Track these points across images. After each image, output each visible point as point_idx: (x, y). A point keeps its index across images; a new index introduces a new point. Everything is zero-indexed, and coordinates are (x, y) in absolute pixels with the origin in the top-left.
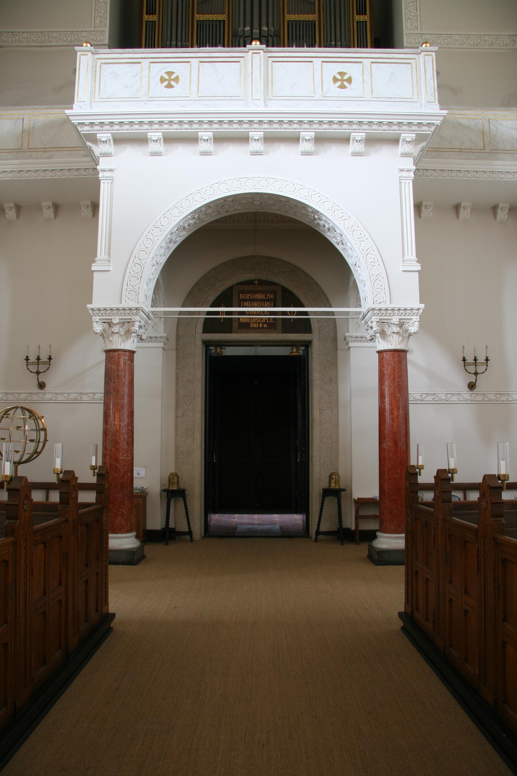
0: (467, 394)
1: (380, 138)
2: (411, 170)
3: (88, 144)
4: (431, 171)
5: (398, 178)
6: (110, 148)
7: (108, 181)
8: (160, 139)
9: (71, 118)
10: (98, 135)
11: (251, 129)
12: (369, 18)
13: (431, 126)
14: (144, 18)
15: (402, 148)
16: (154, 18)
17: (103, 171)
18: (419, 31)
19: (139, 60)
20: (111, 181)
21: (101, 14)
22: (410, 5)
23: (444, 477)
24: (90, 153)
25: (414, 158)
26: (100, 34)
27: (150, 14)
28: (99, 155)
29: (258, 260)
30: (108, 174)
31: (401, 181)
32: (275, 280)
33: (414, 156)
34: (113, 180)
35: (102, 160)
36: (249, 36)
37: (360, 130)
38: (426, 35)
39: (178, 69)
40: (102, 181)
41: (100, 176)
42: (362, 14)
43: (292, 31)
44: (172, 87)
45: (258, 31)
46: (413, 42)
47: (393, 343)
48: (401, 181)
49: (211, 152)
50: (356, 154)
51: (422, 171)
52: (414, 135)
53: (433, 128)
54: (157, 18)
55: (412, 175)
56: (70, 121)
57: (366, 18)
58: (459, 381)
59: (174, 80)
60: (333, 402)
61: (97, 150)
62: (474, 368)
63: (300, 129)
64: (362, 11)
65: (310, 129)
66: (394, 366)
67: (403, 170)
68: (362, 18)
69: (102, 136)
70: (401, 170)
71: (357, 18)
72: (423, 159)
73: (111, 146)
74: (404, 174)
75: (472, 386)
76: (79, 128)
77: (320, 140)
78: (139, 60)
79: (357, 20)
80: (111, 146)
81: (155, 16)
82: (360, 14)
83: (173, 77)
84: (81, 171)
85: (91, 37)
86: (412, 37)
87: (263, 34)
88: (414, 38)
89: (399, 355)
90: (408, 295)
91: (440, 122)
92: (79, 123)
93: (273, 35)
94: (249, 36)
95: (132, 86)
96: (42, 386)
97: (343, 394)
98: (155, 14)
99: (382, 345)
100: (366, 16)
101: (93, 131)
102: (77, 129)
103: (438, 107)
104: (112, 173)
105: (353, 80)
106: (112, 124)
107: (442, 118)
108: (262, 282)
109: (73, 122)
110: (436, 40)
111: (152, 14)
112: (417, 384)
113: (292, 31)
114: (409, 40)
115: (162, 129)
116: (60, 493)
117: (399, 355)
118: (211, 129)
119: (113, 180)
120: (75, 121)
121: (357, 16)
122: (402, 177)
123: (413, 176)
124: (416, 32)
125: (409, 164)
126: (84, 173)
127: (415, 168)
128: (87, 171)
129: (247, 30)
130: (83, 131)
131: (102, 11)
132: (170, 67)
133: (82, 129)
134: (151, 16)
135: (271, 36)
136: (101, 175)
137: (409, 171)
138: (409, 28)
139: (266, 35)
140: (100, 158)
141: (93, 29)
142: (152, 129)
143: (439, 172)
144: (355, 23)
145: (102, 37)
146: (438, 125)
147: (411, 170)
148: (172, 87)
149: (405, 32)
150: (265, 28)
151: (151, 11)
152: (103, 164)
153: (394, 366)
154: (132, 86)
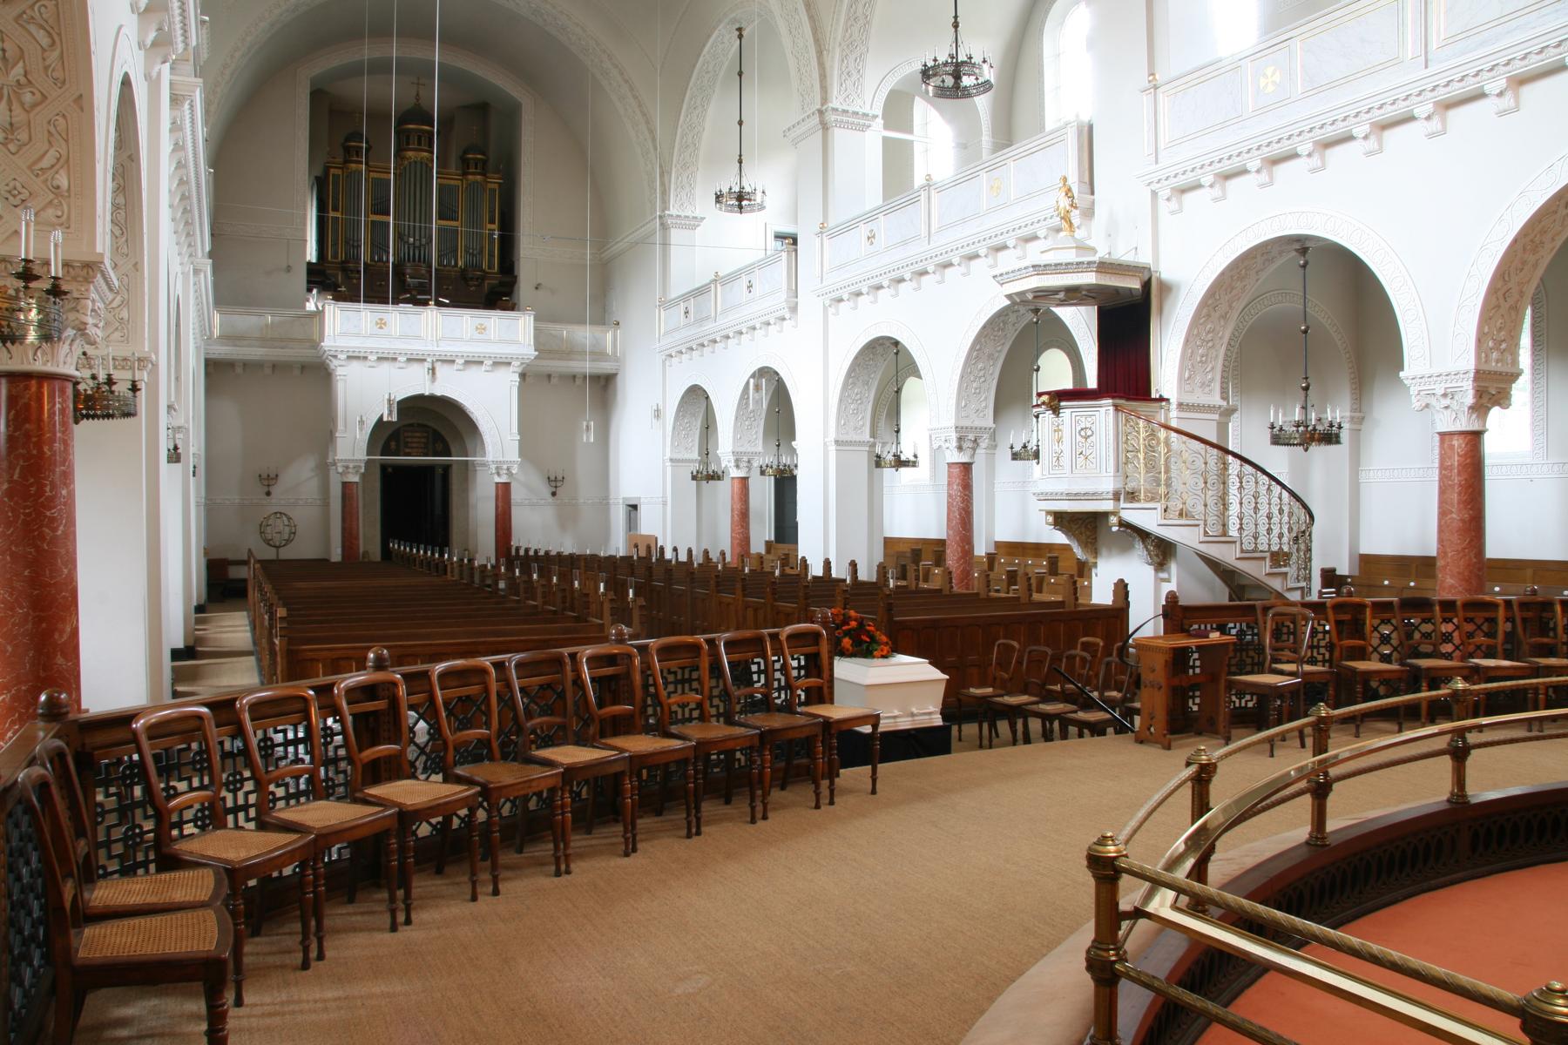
0: (550, 499)
1: (500, 363)
16: (338, 215)
23: (547, 553)
29: (428, 433)
32: (430, 424)
47: (504, 479)
58: (546, 491)
60: (466, 504)
62: (555, 484)
64: (492, 222)
66: (504, 491)
75: (554, 494)
89: (507, 486)
90: (513, 454)
96: (268, 494)
97: (472, 500)
99: (497, 480)
108: (419, 425)
112: (517, 495)
116: (941, 543)
117: (507, 486)
151: (335, 209)
153: (504, 491)
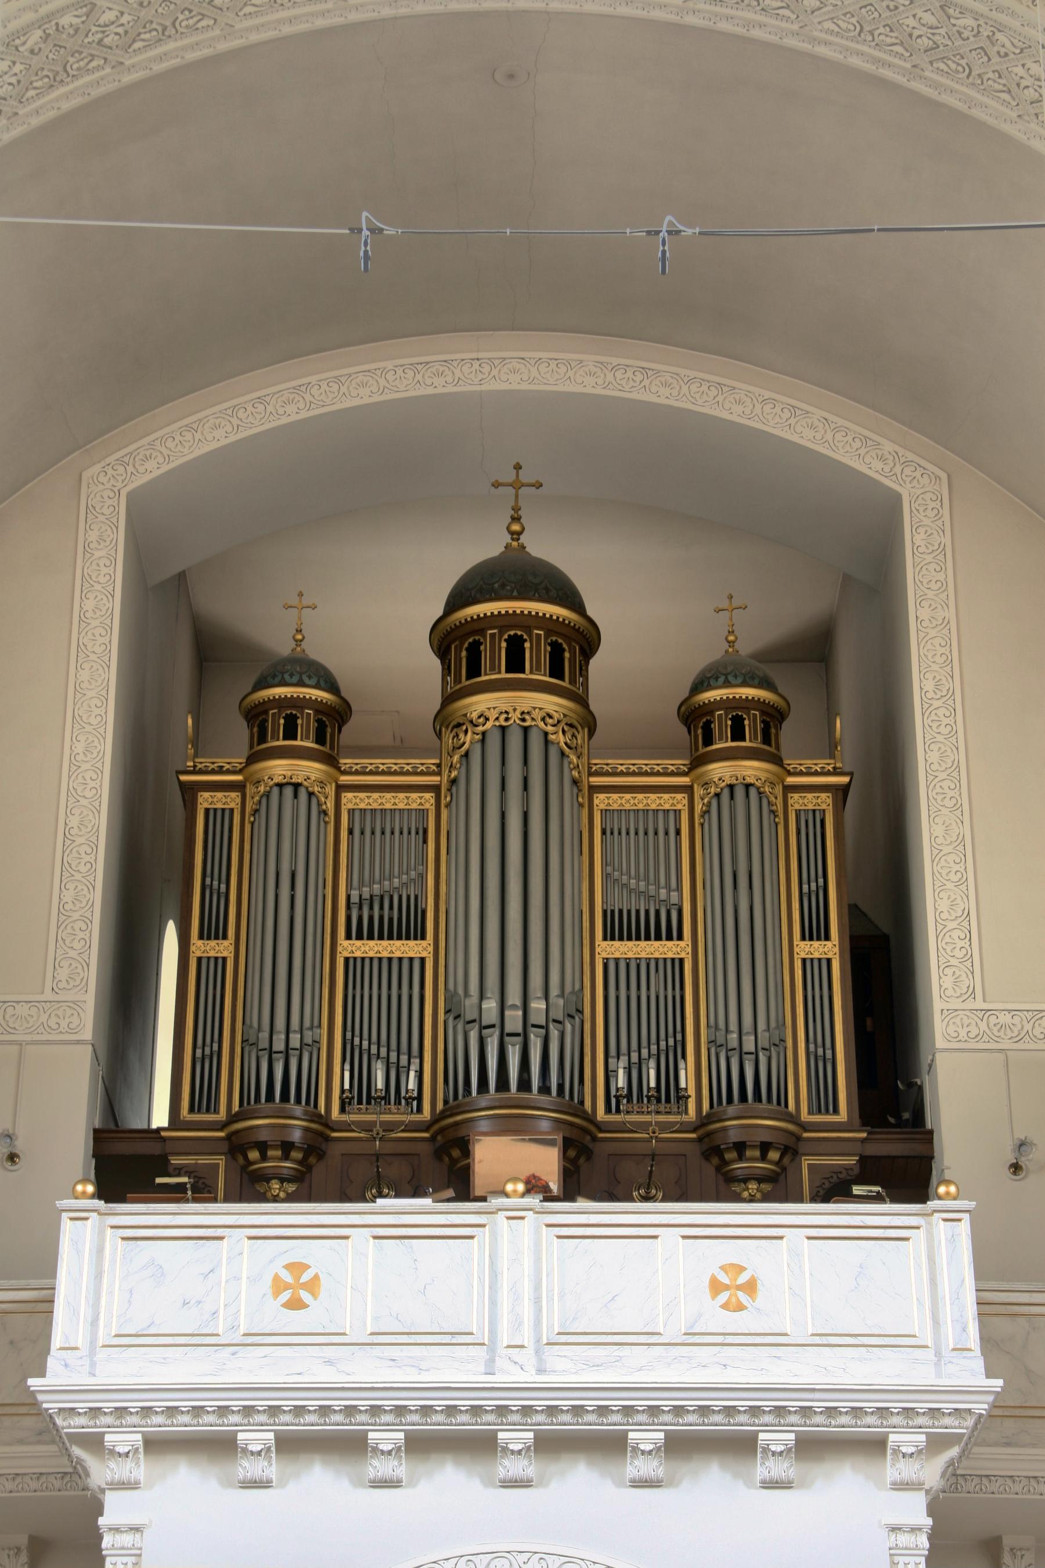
1: (836, 1439)
2: (920, 1529)
3: (77, 1451)
4: (1001, 1481)
5: (888, 1553)
6: (137, 1469)
7: (125, 1559)
8: (269, 1449)
9: (40, 1397)
10: (107, 1438)
11: (502, 1424)
12: (837, 950)
13: (963, 1414)
14: (193, 948)
15: (895, 1470)
16: (223, 948)
17: (116, 1530)
18: (979, 1004)
19: (219, 1232)
20: (133, 1559)
21: (72, 954)
22: (951, 925)
24: (77, 1472)
25: (927, 1492)
26: (69, 1012)
27: (209, 938)
28: (104, 1486)
30: (127, 1539)
31: (896, 1559)
33: (927, 1487)
34: (140, 1555)
35: (110, 1499)
36: (493, 1026)
37: (780, 1425)
38: (1001, 1015)
39: (316, 1255)
40: (108, 1560)
41: (104, 1545)
42: (819, 939)
43: (617, 988)
44: (289, 1267)
45: (520, 1013)
46: (963, 1033)
48: (896, 1559)
49: (400, 1481)
50: (771, 1484)
51: (976, 1480)
52: (923, 1438)
53: (970, 1422)
54: (232, 948)
55: (923, 1541)
56: (36, 1404)
57: (830, 949)
59: (305, 1286)
61: (100, 1472)
63: (628, 1424)
64: (816, 930)
65: (653, 1424)
67: (899, 1529)
68: (817, 949)
69: (121, 1439)
70: (895, 1529)
71: (805, 949)
72: (976, 1450)
73: (137, 1464)
74: (904, 1539)
76: (59, 1421)
77: (680, 1446)
78: (219, 1232)
79: (803, 955)
80: (137, 1464)
81: (226, 943)
82: (811, 939)
83: (306, 1277)
84: (27, 1479)
85: (44, 1018)
86: (958, 1020)
87: (533, 1019)
88: (966, 1021)
91: (986, 1406)
92: (60, 1409)
93: (561, 1019)
94: (493, 1026)
95: (199, 1302)
98: (225, 937)
100: (829, 944)
101: (96, 1426)
102: (54, 1424)
103: (978, 1364)
104: (138, 1536)
105: (759, 1286)
106: (147, 1411)
107: (990, 1398)
109: (45, 1406)
110: (1028, 1027)
111: (217, 938)
113: (617, 988)
114: (951, 1029)
115: (275, 1424)
118: (401, 1424)
119: (140, 1555)
120: (50, 1405)
121: (802, 944)
122: (897, 1547)
123: (927, 1545)
124: (970, 1005)
125: (914, 1510)
126: (34, 1485)
127: (929, 1521)
128: (43, 1479)
129: (489, 1009)
130: (69, 1427)
131: (77, 945)
132: (298, 1251)
133: (65, 1424)
134: (213, 943)
135: (554, 1021)
136: (107, 1541)
137: (914, 1530)
138: (949, 993)
139: (544, 1023)
140: (107, 1492)
141: (48, 995)
142: (249, 1424)
143: (1025, 1482)
144: (798, 965)
145: (76, 1021)
146: (981, 1415)
147: (920, 1529)
148: (289, 1267)
149: (938, 1005)
150: (538, 1005)
152: (116, 1511)
154: (199, 1302)
